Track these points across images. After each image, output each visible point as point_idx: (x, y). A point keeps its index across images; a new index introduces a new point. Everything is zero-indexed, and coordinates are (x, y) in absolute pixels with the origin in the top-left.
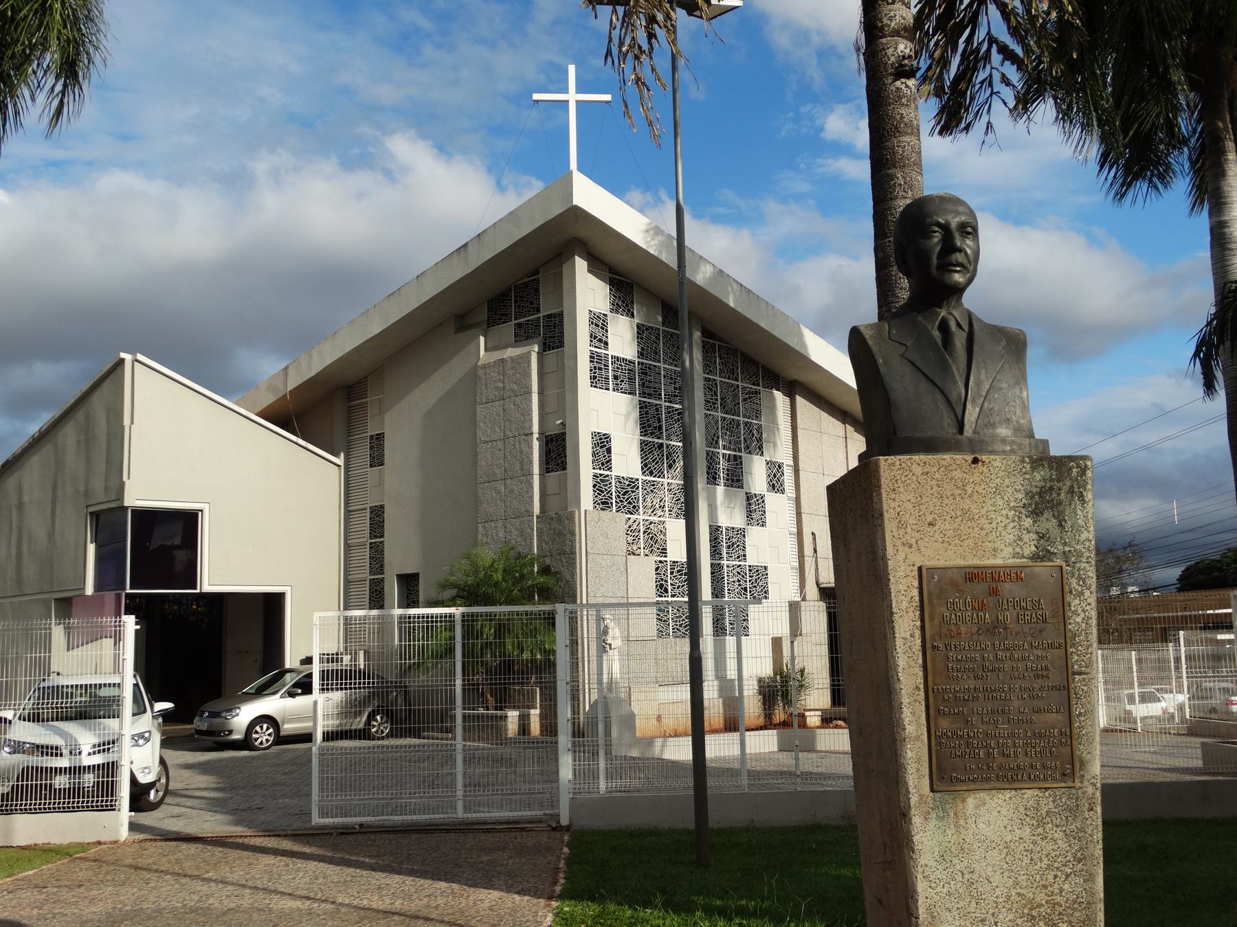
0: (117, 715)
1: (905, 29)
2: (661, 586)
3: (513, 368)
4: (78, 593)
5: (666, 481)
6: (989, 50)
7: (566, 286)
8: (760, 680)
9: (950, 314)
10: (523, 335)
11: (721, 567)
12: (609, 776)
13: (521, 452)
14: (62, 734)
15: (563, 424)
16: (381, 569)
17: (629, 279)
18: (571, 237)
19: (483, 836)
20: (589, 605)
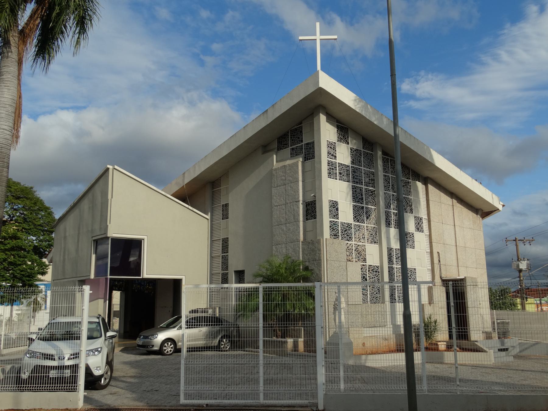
2: (364, 277)
4: (88, 277)
5: (365, 225)
7: (315, 128)
10: (295, 153)
12: (347, 380)
13: (294, 210)
14: (54, 347)
15: (314, 196)
16: (227, 268)
17: (347, 125)
18: (318, 104)
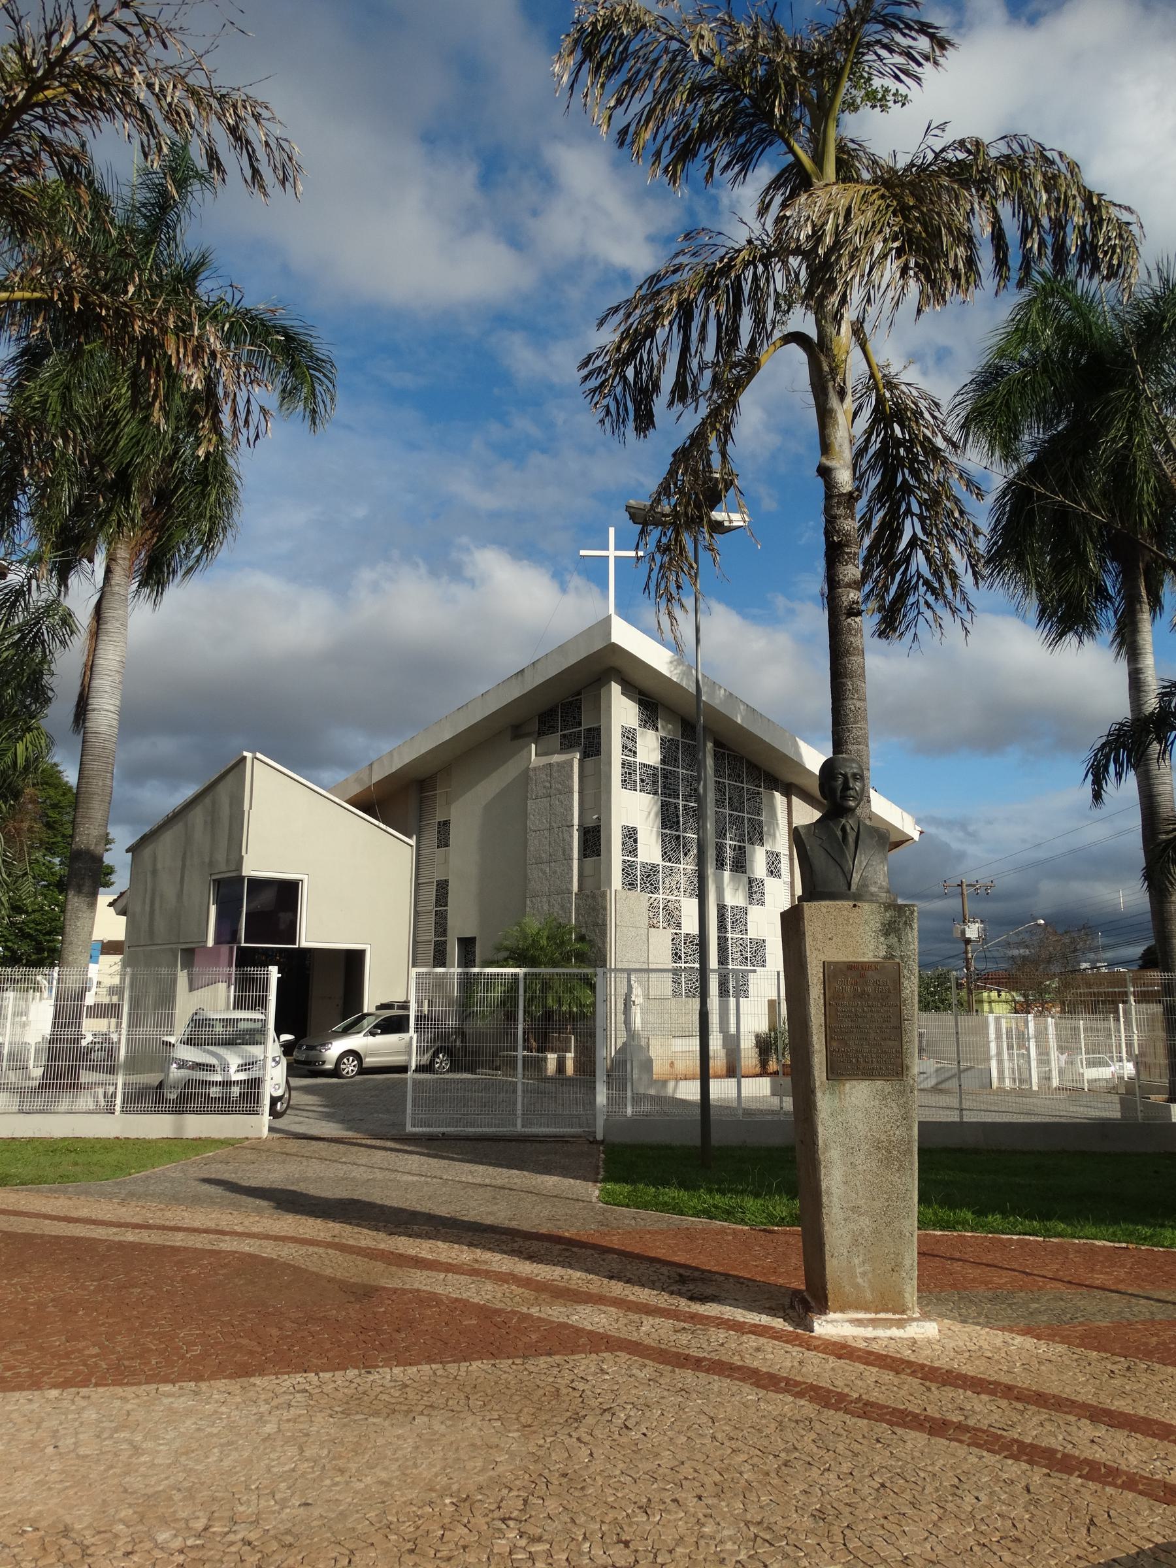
0: (263, 1043)
1: (855, 583)
3: (559, 771)
5: (682, 866)
6: (917, 582)
8: (757, 1036)
9: (850, 823)
10: (567, 745)
11: (726, 939)
15: (598, 818)
17: (654, 700)
18: (607, 667)
19: (538, 1145)
20: (616, 970)
